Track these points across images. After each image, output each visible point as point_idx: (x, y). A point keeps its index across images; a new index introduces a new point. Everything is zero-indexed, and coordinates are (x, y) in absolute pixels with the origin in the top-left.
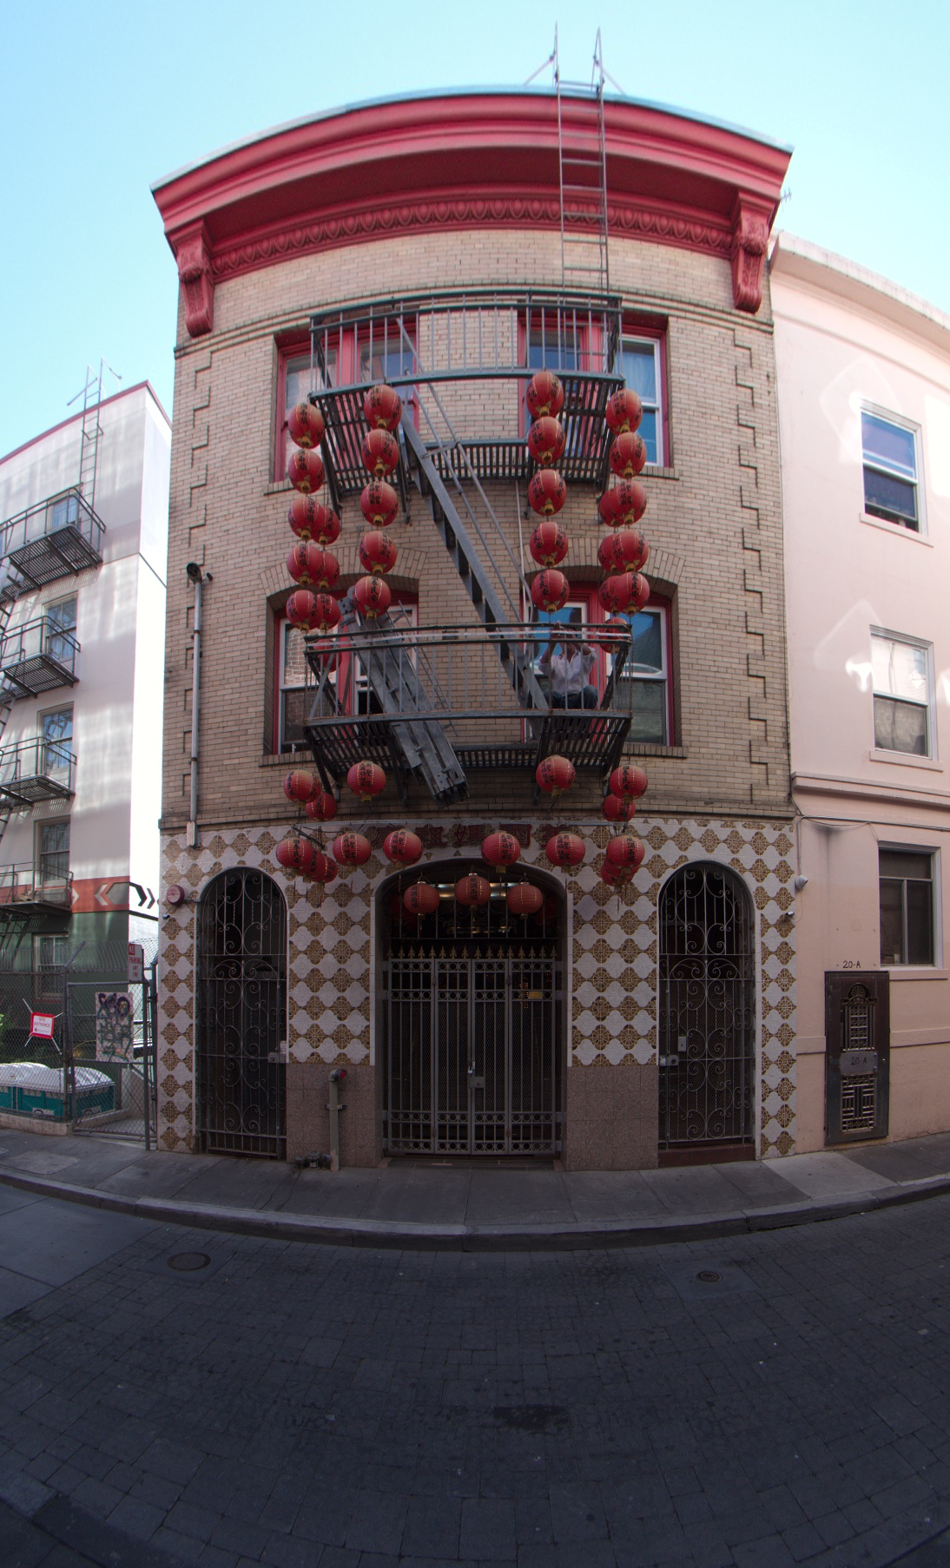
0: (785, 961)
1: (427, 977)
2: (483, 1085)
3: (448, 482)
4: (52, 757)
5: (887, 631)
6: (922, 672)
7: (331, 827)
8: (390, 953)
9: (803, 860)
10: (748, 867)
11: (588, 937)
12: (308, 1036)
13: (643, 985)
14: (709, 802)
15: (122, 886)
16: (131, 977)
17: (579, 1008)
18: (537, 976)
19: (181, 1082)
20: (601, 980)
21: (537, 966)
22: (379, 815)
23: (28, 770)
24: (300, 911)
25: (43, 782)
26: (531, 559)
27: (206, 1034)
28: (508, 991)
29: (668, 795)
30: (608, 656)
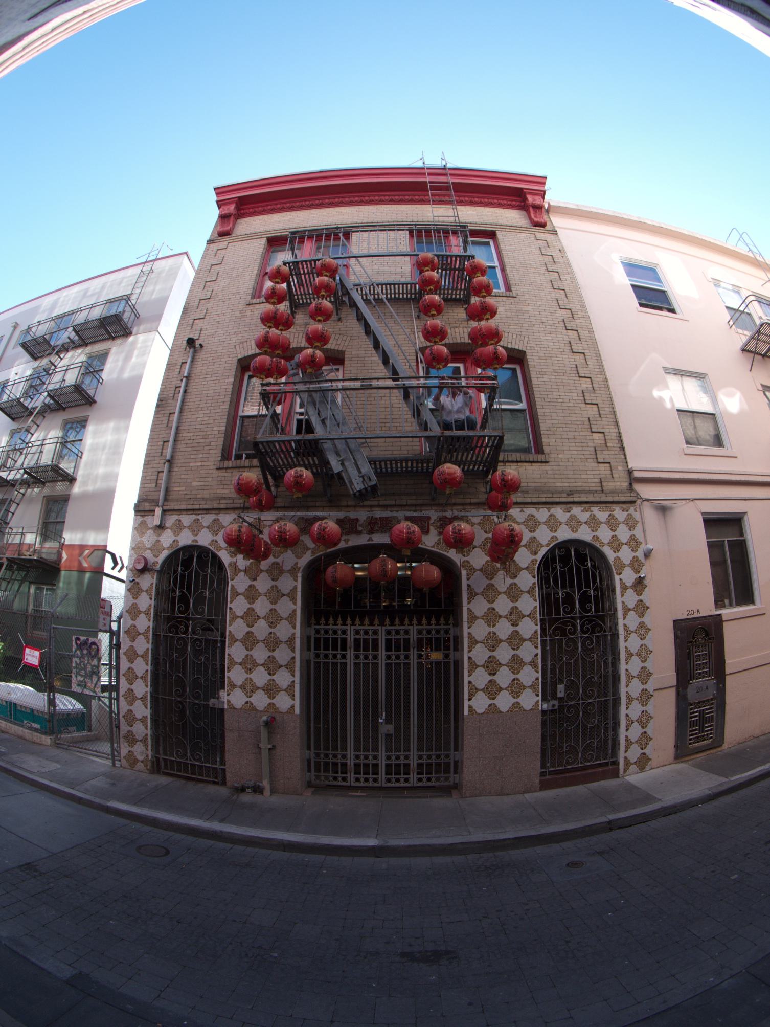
0: (641, 615)
1: (344, 641)
2: (392, 732)
3: (367, 301)
4: (65, 451)
5: (675, 370)
6: (706, 392)
7: (268, 517)
8: (313, 621)
9: (647, 533)
10: (606, 541)
11: (480, 606)
12: (243, 687)
14: (570, 493)
15: (100, 553)
16: (101, 627)
17: (473, 666)
18: (438, 640)
19: (139, 716)
20: (492, 642)
21: (438, 632)
22: (308, 508)
23: (46, 459)
24: (239, 583)
25: (55, 469)
26: (423, 339)
27: (158, 679)
28: (413, 653)
29: (538, 490)
30: (482, 395)
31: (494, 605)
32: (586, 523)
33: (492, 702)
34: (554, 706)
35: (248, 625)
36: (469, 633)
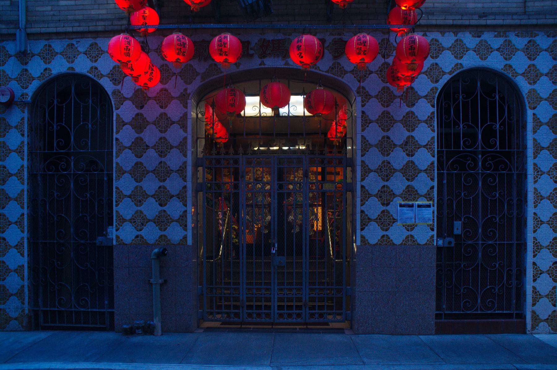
11: (374, 208)
12: (132, 221)
13: (423, 176)
14: (483, 15)
31: (389, 134)
32: (498, 50)
34: (450, 243)
35: (137, 156)
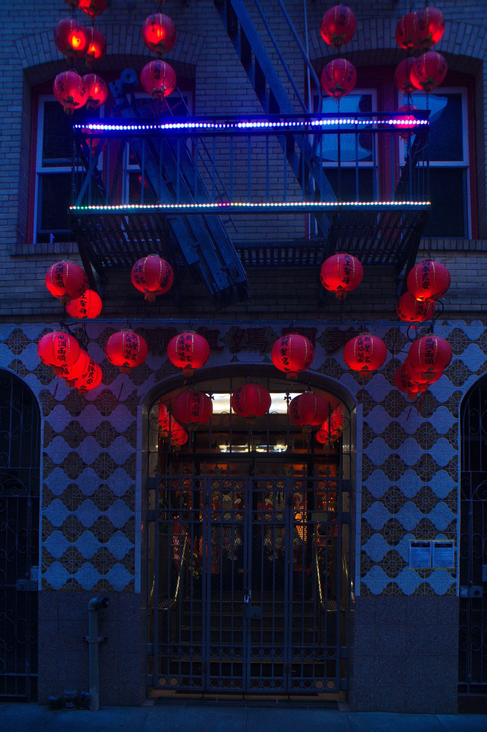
12: (64, 560)
33: (392, 580)
34: (477, 593)
35: (70, 476)
36: (364, 488)
